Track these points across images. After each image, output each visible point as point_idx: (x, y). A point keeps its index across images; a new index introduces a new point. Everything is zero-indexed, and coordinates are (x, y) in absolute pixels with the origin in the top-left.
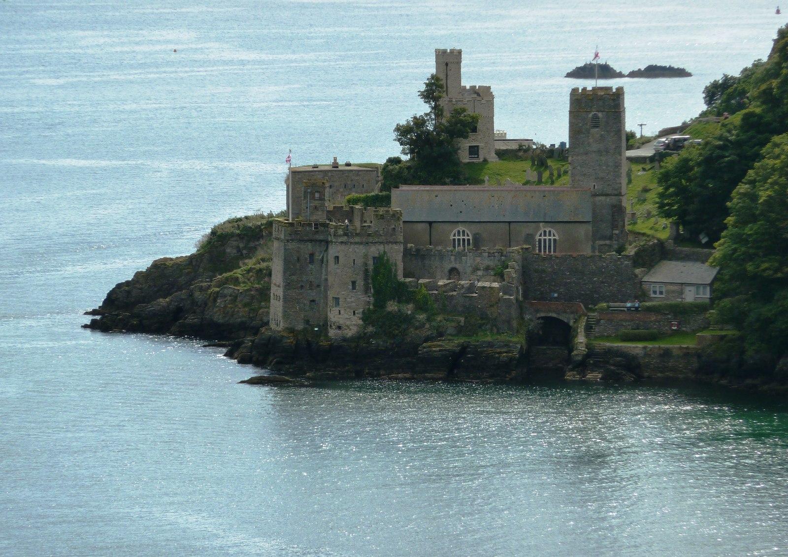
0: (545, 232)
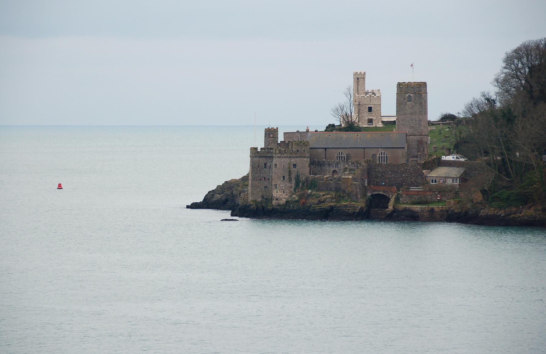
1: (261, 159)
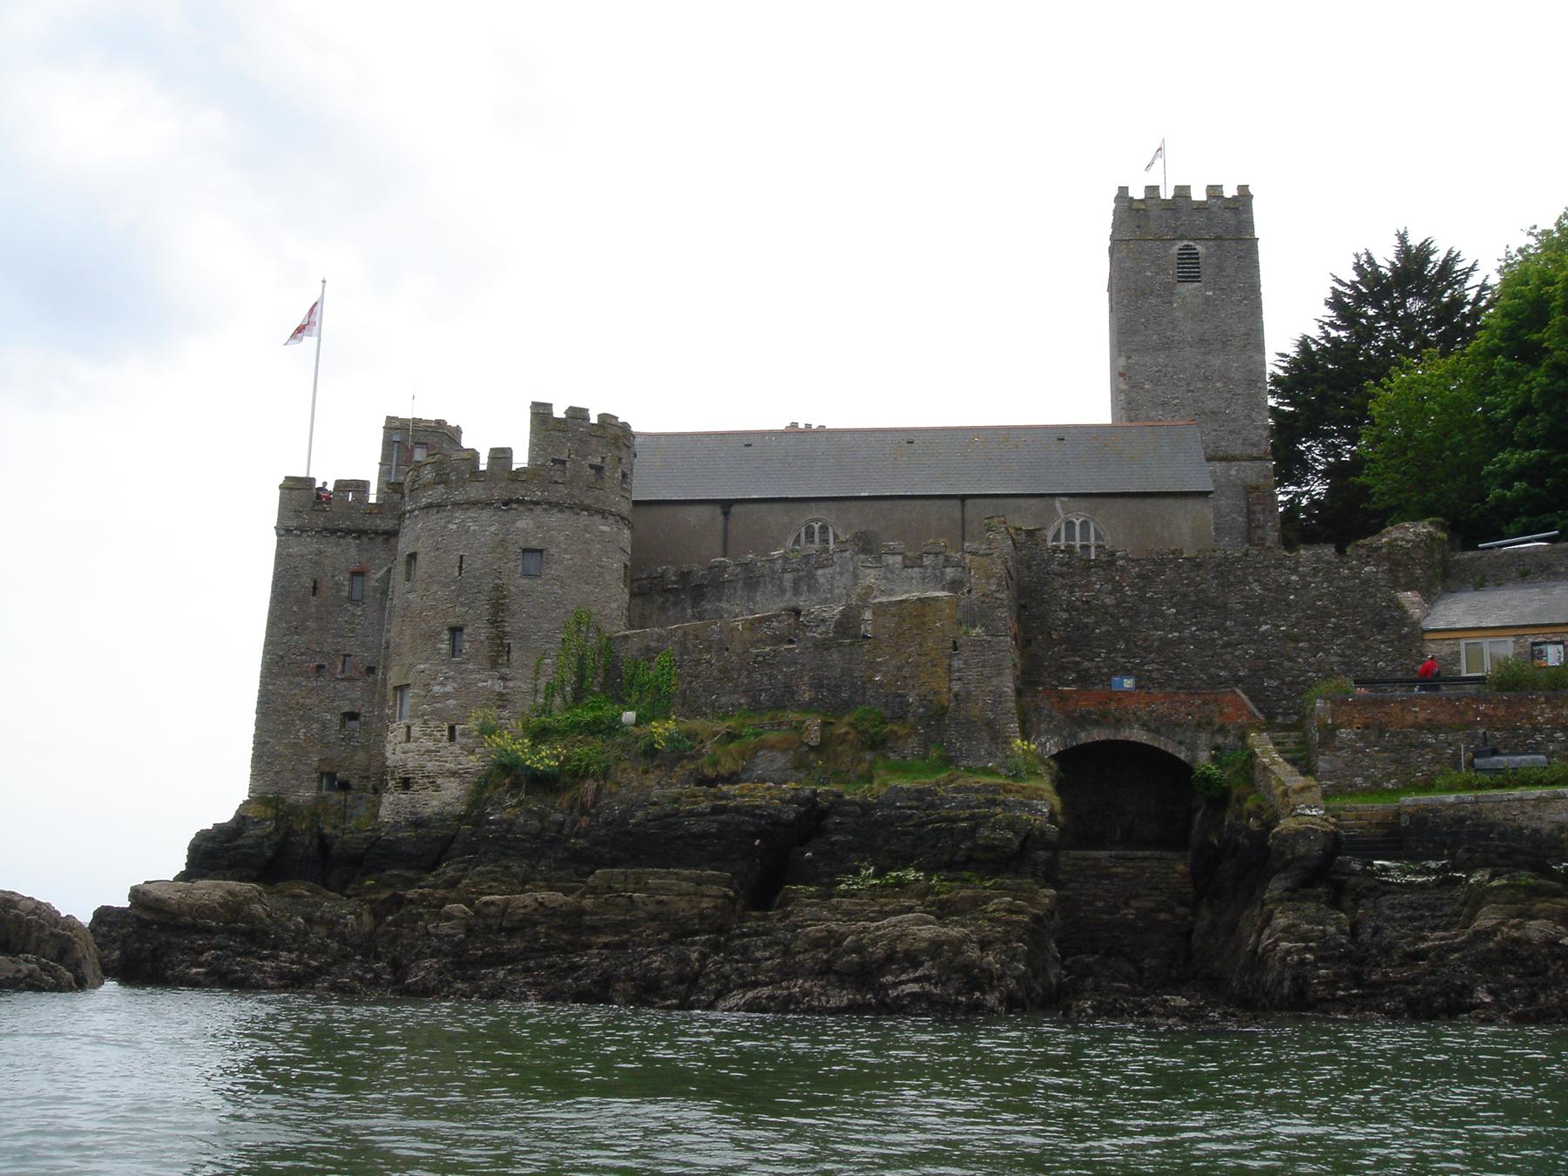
0: (1070, 525)
1: (331, 548)
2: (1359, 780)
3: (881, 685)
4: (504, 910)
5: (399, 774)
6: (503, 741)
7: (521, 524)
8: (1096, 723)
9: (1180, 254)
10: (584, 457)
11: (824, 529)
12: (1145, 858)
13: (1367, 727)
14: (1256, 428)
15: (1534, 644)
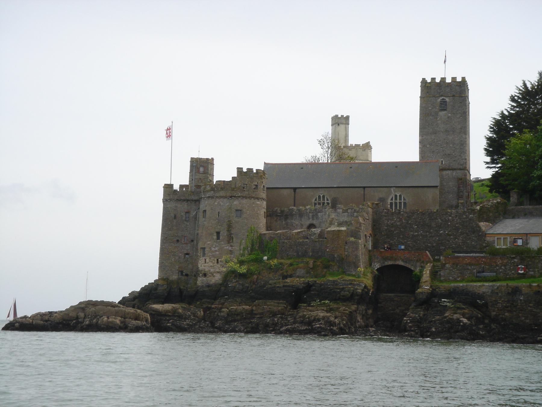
0: (396, 196)
2: (451, 278)
3: (328, 252)
4: (236, 310)
5: (203, 272)
6: (231, 264)
7: (235, 203)
8: (390, 260)
9: (444, 102)
10: (252, 183)
11: (324, 197)
12: (403, 296)
13: (454, 264)
14: (462, 159)
15: (515, 239)
